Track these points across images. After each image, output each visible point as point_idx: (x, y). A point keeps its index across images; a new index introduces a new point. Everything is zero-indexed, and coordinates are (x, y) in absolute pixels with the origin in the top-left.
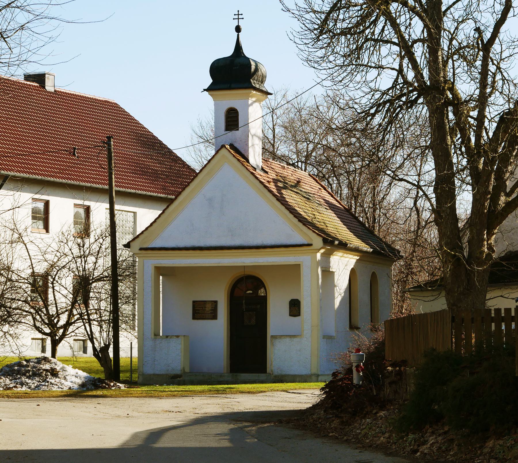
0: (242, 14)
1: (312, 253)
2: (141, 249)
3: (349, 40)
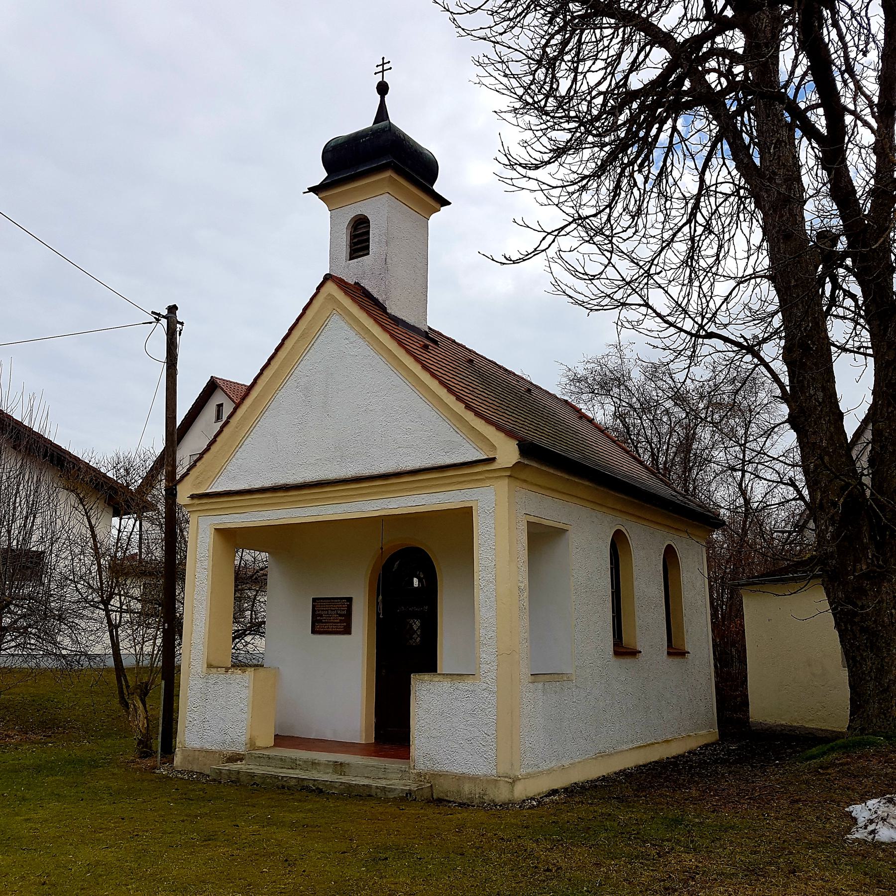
0: (389, 62)
1: (497, 478)
2: (193, 497)
3: (582, 113)
